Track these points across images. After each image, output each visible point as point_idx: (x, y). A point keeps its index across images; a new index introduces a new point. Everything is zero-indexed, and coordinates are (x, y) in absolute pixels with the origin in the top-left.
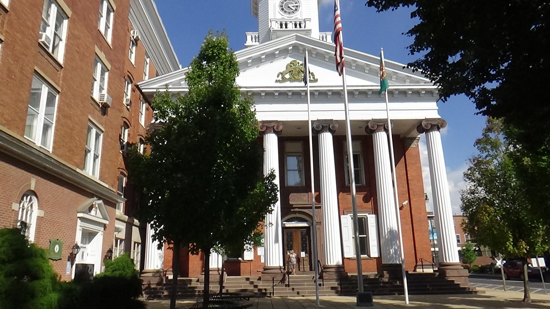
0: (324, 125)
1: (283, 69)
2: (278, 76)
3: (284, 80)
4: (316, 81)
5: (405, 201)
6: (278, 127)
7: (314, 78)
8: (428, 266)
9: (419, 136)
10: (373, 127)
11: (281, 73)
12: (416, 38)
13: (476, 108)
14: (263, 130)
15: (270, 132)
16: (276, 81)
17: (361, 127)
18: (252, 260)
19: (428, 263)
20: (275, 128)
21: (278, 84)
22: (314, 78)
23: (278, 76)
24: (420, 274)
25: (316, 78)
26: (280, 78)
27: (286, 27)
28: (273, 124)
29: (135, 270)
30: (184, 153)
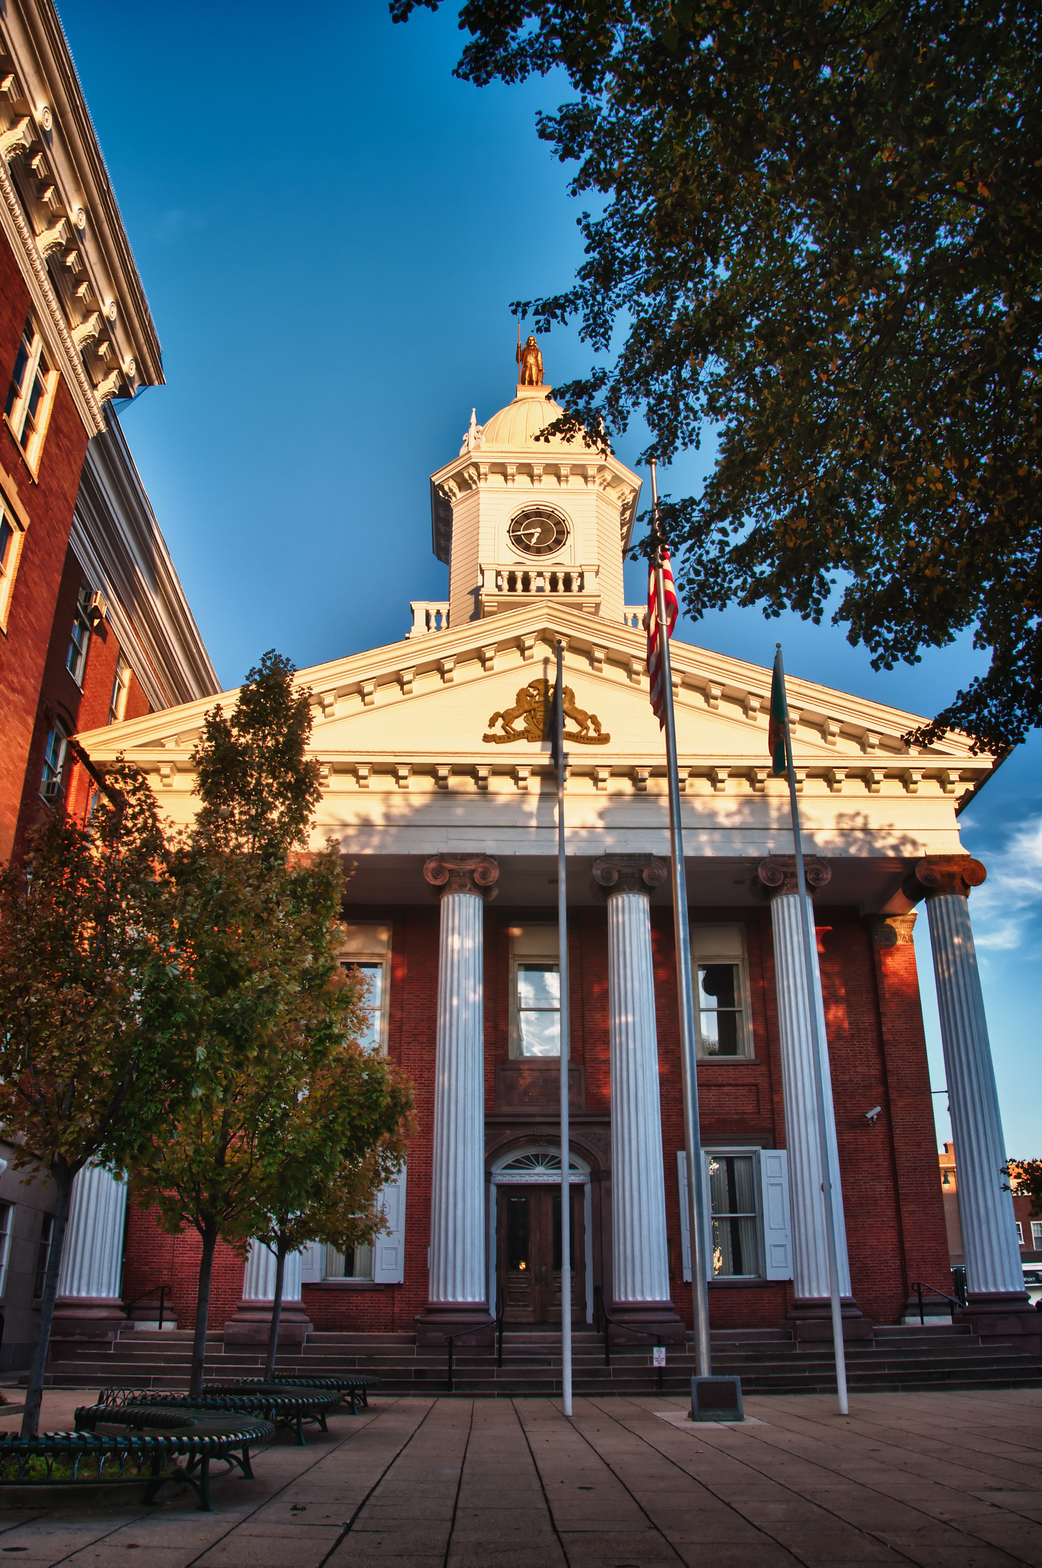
0: (626, 870)
1: (510, 703)
2: (492, 725)
3: (511, 736)
4: (604, 739)
5: (873, 1106)
6: (484, 875)
7: (597, 730)
8: (936, 1309)
9: (913, 911)
10: (771, 880)
11: (502, 716)
12: (285, 692)
13: (461, 26)
14: (438, 883)
15: (461, 888)
16: (487, 738)
17: (741, 882)
18: (399, 1285)
19: (939, 1299)
20: (476, 875)
21: (492, 747)
22: (597, 730)
23: (492, 725)
24: (914, 1330)
25: (603, 731)
26: (498, 730)
27: (581, 588)
28: (470, 866)
29: (350, 1063)
30: (9, 1036)
